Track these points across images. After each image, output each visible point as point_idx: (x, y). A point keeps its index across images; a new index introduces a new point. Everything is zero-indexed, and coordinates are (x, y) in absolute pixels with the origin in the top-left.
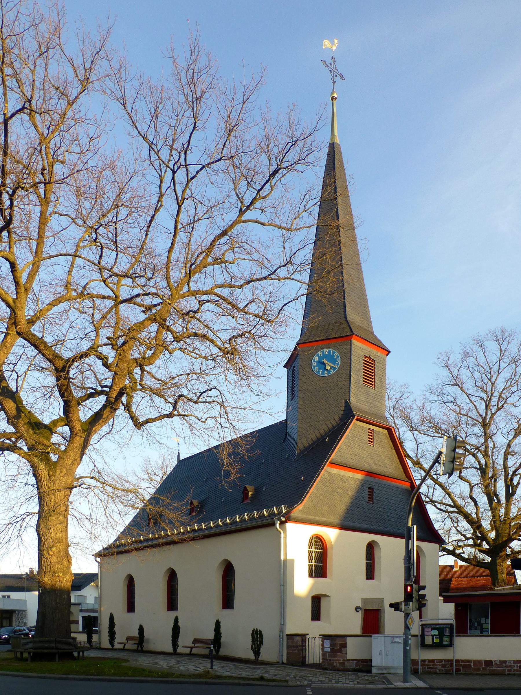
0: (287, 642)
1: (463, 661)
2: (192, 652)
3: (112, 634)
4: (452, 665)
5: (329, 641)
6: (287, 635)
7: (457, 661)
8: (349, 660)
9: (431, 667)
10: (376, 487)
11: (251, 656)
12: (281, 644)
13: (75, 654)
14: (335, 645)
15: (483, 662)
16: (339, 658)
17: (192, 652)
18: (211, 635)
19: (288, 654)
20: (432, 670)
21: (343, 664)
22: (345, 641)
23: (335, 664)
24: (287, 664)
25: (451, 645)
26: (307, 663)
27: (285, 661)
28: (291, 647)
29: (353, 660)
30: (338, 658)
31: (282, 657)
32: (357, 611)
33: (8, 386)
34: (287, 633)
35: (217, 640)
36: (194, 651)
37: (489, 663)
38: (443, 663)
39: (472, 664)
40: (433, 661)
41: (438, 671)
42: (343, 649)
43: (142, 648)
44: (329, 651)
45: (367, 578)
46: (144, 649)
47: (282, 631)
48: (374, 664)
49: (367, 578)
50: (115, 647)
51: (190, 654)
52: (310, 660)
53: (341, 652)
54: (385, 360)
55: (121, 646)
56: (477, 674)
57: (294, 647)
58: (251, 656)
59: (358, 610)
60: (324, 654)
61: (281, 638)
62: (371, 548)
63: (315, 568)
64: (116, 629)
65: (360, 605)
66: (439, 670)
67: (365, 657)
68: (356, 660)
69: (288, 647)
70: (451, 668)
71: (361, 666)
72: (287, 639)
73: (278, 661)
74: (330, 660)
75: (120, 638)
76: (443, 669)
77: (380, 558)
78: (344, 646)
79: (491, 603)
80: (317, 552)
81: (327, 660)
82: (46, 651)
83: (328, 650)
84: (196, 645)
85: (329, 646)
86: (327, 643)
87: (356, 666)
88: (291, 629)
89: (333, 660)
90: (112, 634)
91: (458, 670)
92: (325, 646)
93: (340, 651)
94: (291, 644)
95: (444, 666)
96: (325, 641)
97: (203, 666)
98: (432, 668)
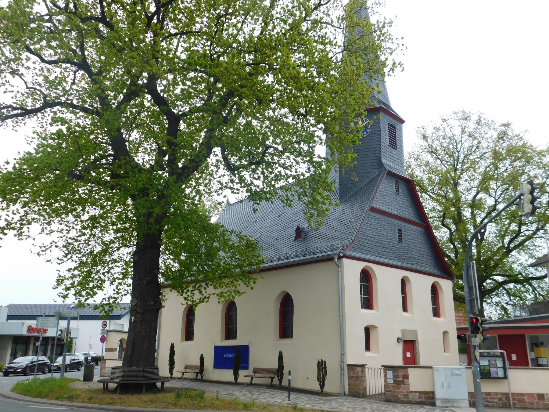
0: (348, 372)
1: (518, 394)
2: (253, 382)
3: (172, 363)
4: (508, 399)
5: (391, 372)
6: (348, 365)
7: (512, 394)
8: (412, 392)
9: (489, 400)
10: (403, 229)
11: (316, 387)
12: (342, 375)
13: (159, 385)
15: (536, 395)
16: (403, 389)
17: (253, 382)
18: (275, 365)
19: (349, 385)
20: (489, 404)
21: (407, 396)
22: (407, 371)
23: (399, 396)
24: (349, 395)
25: (505, 377)
26: (368, 394)
27: (347, 392)
28: (353, 377)
29: (415, 392)
31: (344, 388)
32: (399, 342)
34: (348, 363)
35: (280, 371)
36: (255, 381)
37: (541, 397)
38: (499, 396)
39: (526, 398)
40: (489, 394)
41: (496, 405)
42: (405, 380)
43: (202, 377)
44: (121, 365)
46: (204, 378)
47: (342, 361)
48: (438, 395)
50: (173, 376)
51: (251, 384)
52: (370, 390)
53: (404, 384)
54: (401, 128)
55: (180, 375)
56: (532, 408)
57: (356, 377)
58: (316, 387)
59: (399, 341)
60: (387, 385)
61: (342, 369)
62: (404, 282)
64: (175, 358)
65: (400, 336)
66: (497, 403)
67: (427, 388)
68: (419, 392)
69: (350, 378)
70: (507, 402)
71: (424, 399)
72: (348, 370)
73: (340, 392)
74: (394, 392)
75: (178, 367)
76: (500, 402)
77: (411, 293)
78: (406, 377)
79: (499, 336)
81: (391, 391)
82: (133, 382)
83: (391, 381)
84: (257, 375)
85: (392, 377)
86: (390, 374)
87: (419, 398)
88: (350, 360)
89: (397, 392)
90: (172, 363)
91: (514, 404)
92: (388, 377)
93: (403, 382)
94: (352, 375)
95: (500, 399)
96: (388, 372)
98: (489, 402)
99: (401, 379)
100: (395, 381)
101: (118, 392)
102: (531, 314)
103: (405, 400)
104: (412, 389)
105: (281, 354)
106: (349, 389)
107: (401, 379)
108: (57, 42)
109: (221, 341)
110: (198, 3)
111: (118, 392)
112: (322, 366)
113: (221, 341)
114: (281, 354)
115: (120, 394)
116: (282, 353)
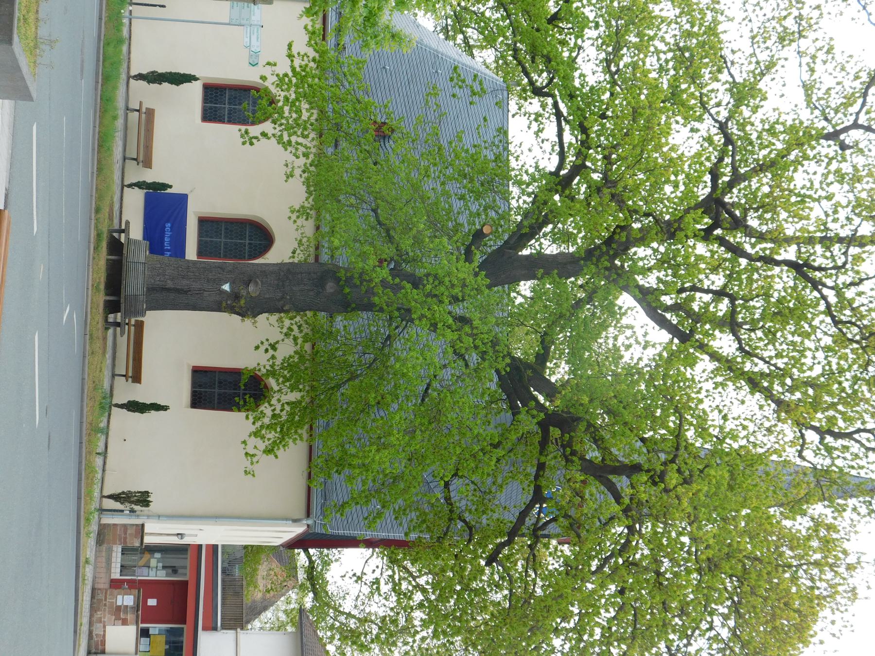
0: (133, 525)
6: (143, 525)
8: (104, 627)
14: (126, 612)
16: (108, 617)
22: (132, 624)
29: (105, 631)
30: (108, 616)
33: (372, 311)
42: (120, 622)
45: (200, 374)
49: (200, 374)
63: (211, 102)
68: (104, 635)
72: (137, 525)
74: (105, 605)
78: (125, 622)
80: (221, 103)
81: (106, 600)
85: (125, 604)
89: (105, 610)
93: (118, 618)
94: (129, 532)
97: (121, 104)
99: (122, 616)
100: (119, 608)
101: (110, 257)
102: (204, 222)
103: (95, 619)
104: (110, 629)
105: (164, 408)
106: (109, 525)
107: (122, 616)
108: (571, 608)
109: (195, 213)
110: (790, 2)
111: (110, 257)
112: (143, 499)
113: (195, 213)
114: (164, 408)
115: (107, 260)
116: (166, 410)
